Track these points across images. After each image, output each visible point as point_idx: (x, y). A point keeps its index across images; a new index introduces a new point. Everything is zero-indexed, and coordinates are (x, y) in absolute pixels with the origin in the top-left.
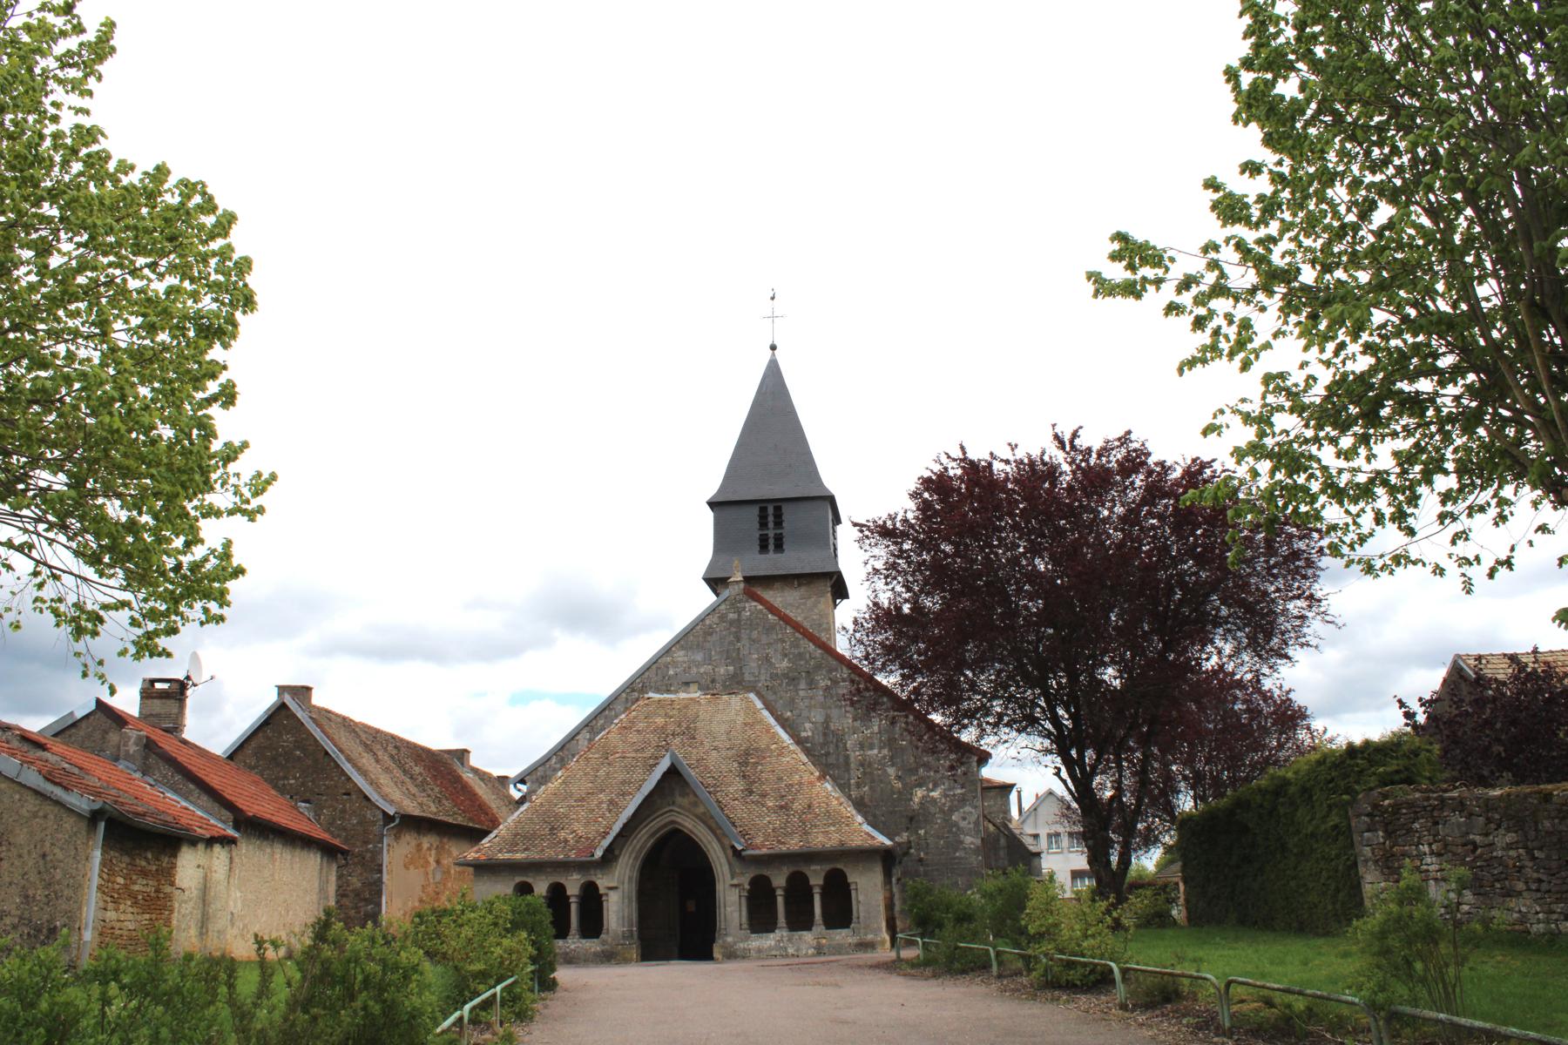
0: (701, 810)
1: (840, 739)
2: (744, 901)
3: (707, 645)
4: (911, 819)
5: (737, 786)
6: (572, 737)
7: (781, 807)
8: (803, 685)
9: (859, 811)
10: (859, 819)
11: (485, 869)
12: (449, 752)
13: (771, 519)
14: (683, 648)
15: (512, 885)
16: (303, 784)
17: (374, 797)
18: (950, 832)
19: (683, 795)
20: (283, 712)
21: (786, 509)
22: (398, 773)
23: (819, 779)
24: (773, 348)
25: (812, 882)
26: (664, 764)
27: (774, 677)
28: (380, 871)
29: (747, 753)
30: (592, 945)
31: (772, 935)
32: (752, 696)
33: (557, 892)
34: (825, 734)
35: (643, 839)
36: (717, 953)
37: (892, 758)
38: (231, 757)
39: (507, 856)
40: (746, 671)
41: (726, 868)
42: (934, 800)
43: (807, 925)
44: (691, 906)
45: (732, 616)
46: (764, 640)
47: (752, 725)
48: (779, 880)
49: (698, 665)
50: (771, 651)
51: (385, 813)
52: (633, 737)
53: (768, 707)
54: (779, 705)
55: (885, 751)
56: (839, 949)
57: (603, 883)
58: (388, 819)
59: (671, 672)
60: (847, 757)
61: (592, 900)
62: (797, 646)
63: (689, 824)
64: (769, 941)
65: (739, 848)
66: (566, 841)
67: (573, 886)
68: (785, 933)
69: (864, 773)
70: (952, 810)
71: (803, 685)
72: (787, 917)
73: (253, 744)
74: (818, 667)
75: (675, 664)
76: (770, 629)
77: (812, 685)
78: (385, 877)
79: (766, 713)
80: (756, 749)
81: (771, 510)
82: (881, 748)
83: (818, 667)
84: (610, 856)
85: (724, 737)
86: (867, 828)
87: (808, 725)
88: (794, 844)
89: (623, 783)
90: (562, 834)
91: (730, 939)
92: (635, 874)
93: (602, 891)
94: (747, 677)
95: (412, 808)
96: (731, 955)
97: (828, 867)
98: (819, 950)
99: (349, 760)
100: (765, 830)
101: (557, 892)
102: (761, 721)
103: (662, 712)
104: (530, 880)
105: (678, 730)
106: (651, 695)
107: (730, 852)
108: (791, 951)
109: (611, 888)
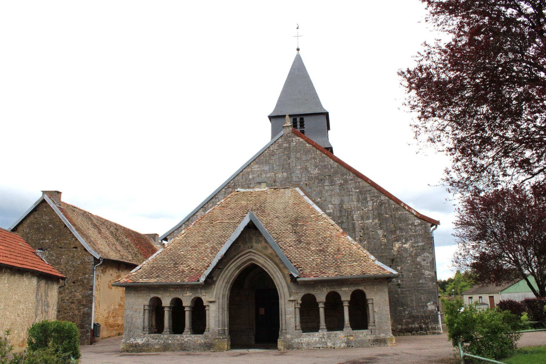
0: (270, 251)
1: (349, 213)
2: (298, 311)
3: (271, 161)
4: (393, 260)
5: (291, 238)
6: (194, 214)
7: (320, 251)
8: (327, 183)
9: (372, 253)
10: (372, 257)
11: (132, 288)
12: (149, 235)
13: (298, 123)
14: (257, 163)
15: (149, 298)
16: (53, 243)
17: (89, 249)
18: (416, 268)
19: (258, 242)
20: (44, 204)
21: (306, 119)
22: (112, 240)
23: (343, 234)
24: (298, 50)
25: (343, 299)
26: (245, 222)
27: (310, 179)
28: (92, 290)
29: (296, 219)
30: (199, 339)
31: (316, 334)
32: (298, 189)
33: (177, 304)
34: (340, 211)
35: (232, 271)
36: (280, 344)
37: (380, 224)
38: (15, 230)
39: (145, 280)
40: (294, 175)
41: (286, 290)
42: (406, 249)
43: (340, 327)
44: (262, 311)
45: (285, 145)
46: (304, 158)
47: (298, 204)
48: (321, 297)
49: (266, 173)
50: (308, 164)
51: (95, 258)
52: (228, 212)
53: (307, 194)
54: (313, 194)
55: (376, 221)
57: (206, 298)
58: (96, 261)
59: (251, 177)
60: (354, 224)
61: (199, 308)
62: (323, 161)
63: (261, 261)
64: (314, 338)
65: (295, 276)
66: (183, 271)
67: (187, 300)
68: (325, 332)
69: (364, 234)
70: (417, 255)
71: (327, 183)
72: (326, 322)
73: (28, 221)
74: (336, 173)
75: (253, 172)
76: (307, 152)
77: (332, 183)
78: (95, 293)
79: (306, 198)
80: (302, 217)
81: (298, 119)
82: (373, 219)
83: (336, 173)
84: (210, 281)
85: (282, 211)
86: (378, 263)
87: (330, 206)
88: (331, 274)
89: (221, 237)
90: (181, 267)
91: (288, 336)
92: (227, 293)
94: (295, 179)
95: (113, 256)
96: (289, 347)
97: (353, 289)
99: (77, 229)
100: (312, 267)
101: (177, 304)
102: (304, 202)
103: (245, 198)
104: (159, 296)
105: (254, 208)
106: (239, 189)
107: (289, 279)
108: (329, 344)
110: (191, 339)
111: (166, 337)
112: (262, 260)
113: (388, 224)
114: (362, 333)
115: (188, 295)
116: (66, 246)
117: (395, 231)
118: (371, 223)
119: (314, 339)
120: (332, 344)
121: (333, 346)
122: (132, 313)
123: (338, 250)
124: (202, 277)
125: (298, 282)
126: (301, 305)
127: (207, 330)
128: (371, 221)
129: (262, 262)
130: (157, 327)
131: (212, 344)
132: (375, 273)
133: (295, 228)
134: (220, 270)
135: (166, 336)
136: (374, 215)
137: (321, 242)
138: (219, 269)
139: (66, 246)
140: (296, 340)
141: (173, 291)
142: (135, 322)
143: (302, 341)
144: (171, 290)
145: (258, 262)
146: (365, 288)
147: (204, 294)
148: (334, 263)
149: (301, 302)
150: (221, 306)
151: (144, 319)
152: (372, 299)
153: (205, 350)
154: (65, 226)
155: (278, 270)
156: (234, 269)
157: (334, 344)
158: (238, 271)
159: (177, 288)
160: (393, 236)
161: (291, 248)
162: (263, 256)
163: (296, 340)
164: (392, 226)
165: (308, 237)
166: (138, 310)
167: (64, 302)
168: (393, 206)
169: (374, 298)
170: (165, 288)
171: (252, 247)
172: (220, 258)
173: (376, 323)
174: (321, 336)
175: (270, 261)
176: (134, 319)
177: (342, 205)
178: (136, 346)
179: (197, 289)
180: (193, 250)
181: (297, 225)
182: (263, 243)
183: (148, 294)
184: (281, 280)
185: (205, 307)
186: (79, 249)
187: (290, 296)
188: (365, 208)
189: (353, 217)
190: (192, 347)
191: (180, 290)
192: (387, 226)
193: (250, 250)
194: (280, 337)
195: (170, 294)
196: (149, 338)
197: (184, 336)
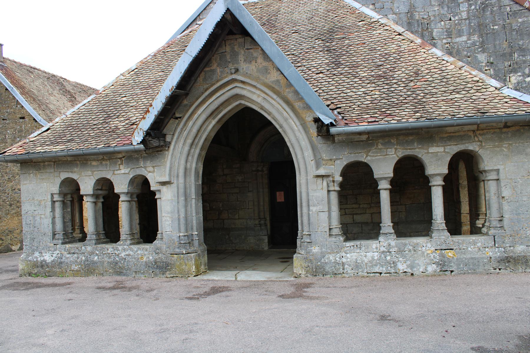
0: (274, 76)
2: (334, 197)
15: (58, 182)
19: (249, 60)
25: (430, 170)
29: (331, 31)
30: (145, 252)
31: (373, 244)
33: (105, 188)
37: (482, 44)
41: (309, 153)
48: (383, 168)
55: (475, 38)
56: (472, 268)
57: (155, 176)
64: (367, 253)
67: (121, 180)
72: (393, 213)
80: (341, 28)
82: (470, 34)
84: (157, 137)
88: (406, 118)
90: (115, 123)
91: (315, 250)
93: (153, 187)
97: (454, 149)
98: (444, 268)
101: (105, 188)
104: (75, 176)
107: (313, 130)
109: (164, 184)
110: (131, 253)
111: (92, 250)
112: (259, 96)
113: (497, 42)
114: (475, 243)
115: (123, 171)
116: (10, 117)
117: (511, 55)
118: (466, 42)
119: (369, 255)
120: (408, 266)
121: (409, 270)
122: (33, 208)
123: (417, 74)
124: (136, 134)
125: (333, 136)
126: (341, 185)
127: (159, 236)
128: (464, 38)
129: (259, 100)
130: (73, 232)
131: (167, 265)
132: (510, 111)
133: (328, 44)
134: (177, 121)
135: (89, 248)
136: (470, 26)
137: (380, 63)
138: (177, 118)
139: (10, 117)
140: (332, 258)
141: (97, 166)
142: (40, 224)
143: (344, 260)
144: (94, 163)
145: (252, 101)
146: (481, 146)
147: (151, 169)
148: (409, 96)
149: (340, 179)
150: (182, 191)
151: (54, 218)
152: (498, 171)
153: (156, 275)
154: (7, 89)
155: (292, 114)
156: (204, 117)
157: (412, 267)
158: (214, 122)
159: (103, 159)
160: (507, 64)
161: (321, 75)
162: (259, 86)
163: (332, 258)
164: (505, 45)
165: (354, 56)
166: (43, 203)
167: (16, 193)
168: (508, 9)
169: (501, 167)
170: (81, 159)
171: (237, 71)
172: (168, 93)
173: (506, 222)
174: (383, 249)
175: (275, 97)
176: (38, 218)
177: (412, 14)
178: (42, 266)
179: (137, 159)
180: (142, 93)
181: (332, 40)
182: (260, 60)
183: (56, 174)
184: (298, 134)
185: (154, 193)
186: (27, 119)
187: (318, 167)
188: (454, 17)
189: (432, 33)
190: (134, 269)
191: (108, 163)
192: (495, 47)
193: (234, 76)
194: (298, 250)
195: (93, 172)
196: (63, 252)
197: (120, 248)
